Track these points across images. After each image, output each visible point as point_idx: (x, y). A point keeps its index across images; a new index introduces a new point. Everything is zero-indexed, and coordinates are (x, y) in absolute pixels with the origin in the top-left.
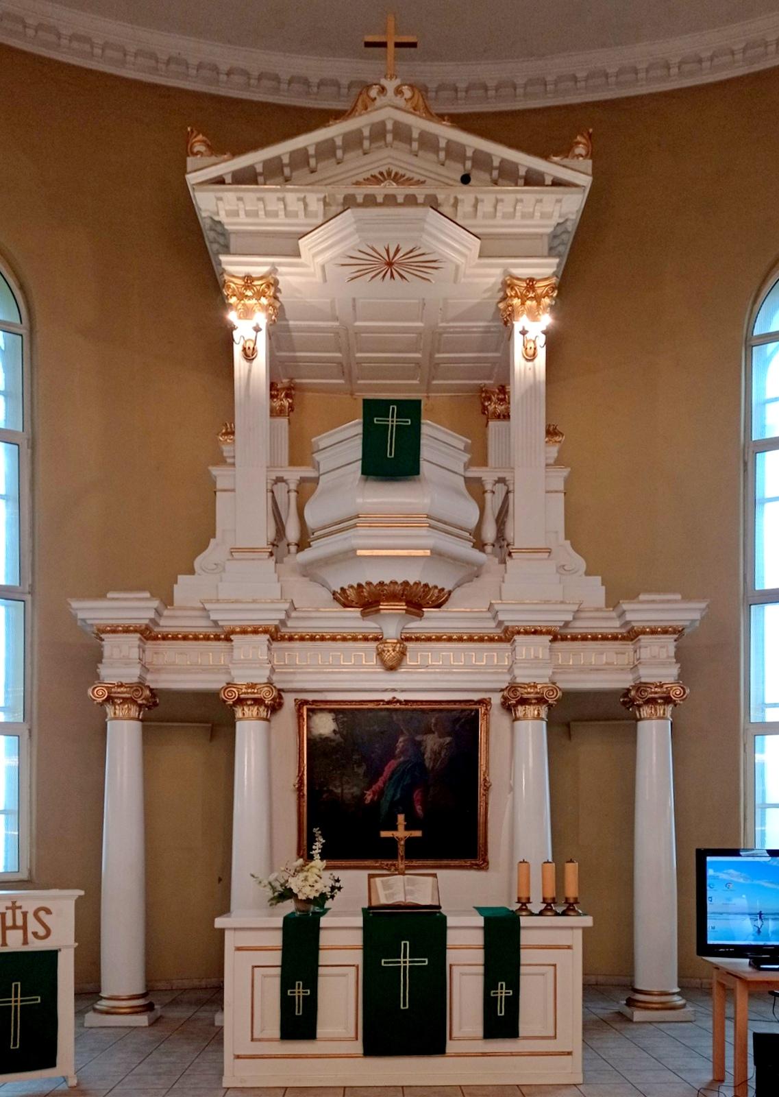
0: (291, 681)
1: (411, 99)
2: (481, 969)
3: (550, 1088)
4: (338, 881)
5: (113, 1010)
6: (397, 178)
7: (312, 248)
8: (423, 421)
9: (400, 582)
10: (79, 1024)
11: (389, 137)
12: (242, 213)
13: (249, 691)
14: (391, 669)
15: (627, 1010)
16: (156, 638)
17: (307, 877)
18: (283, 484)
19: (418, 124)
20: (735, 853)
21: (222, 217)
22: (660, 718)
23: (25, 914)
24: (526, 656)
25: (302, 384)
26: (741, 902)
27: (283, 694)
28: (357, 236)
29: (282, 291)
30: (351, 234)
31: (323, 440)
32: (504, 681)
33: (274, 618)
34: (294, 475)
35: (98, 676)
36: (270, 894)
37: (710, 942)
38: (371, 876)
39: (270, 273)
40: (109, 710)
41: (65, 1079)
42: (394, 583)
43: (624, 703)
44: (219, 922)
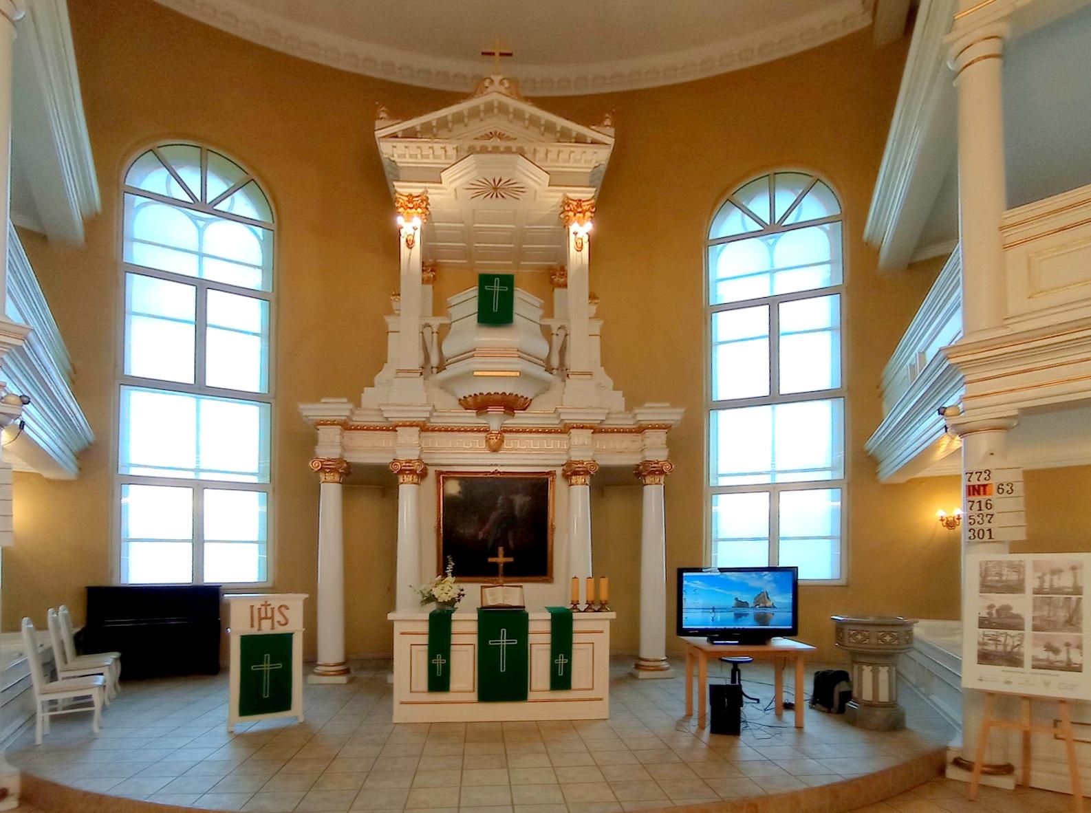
0: (433, 458)
1: (509, 88)
2: (549, 647)
3: (589, 722)
4: (462, 590)
5: (327, 673)
6: (500, 136)
7: (450, 178)
8: (515, 288)
10: (305, 682)
11: (496, 111)
12: (407, 156)
13: (407, 464)
15: (635, 671)
16: (350, 429)
17: (443, 587)
18: (430, 328)
19: (514, 104)
20: (700, 570)
21: (396, 158)
22: (657, 484)
23: (273, 609)
25: (440, 262)
26: (701, 602)
27: (427, 467)
28: (475, 171)
29: (431, 204)
30: (473, 170)
31: (454, 300)
32: (563, 459)
33: (423, 416)
34: (436, 322)
35: (314, 453)
36: (420, 598)
37: (684, 627)
38: (474, 645)
39: (423, 193)
40: (322, 476)
41: (297, 718)
42: (496, 393)
43: (636, 474)
44: (391, 616)
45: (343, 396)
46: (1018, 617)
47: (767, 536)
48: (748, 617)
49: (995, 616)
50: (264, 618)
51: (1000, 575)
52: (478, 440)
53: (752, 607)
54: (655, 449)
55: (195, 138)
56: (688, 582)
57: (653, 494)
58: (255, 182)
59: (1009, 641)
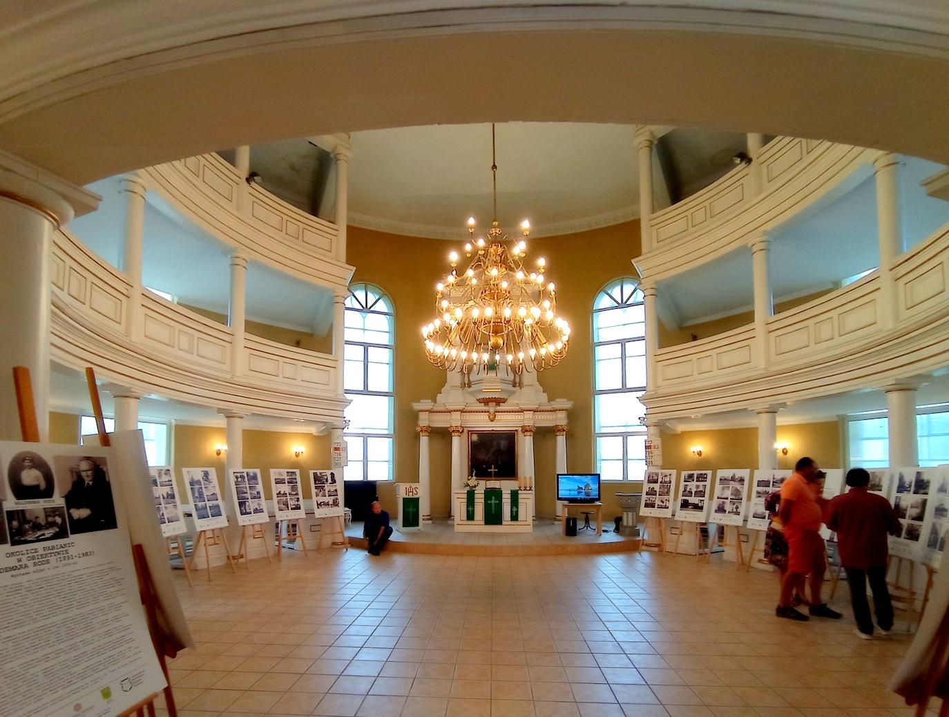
14: (492, 421)
45: (429, 399)
52: (485, 417)
54: (561, 419)
55: (364, 280)
57: (561, 440)
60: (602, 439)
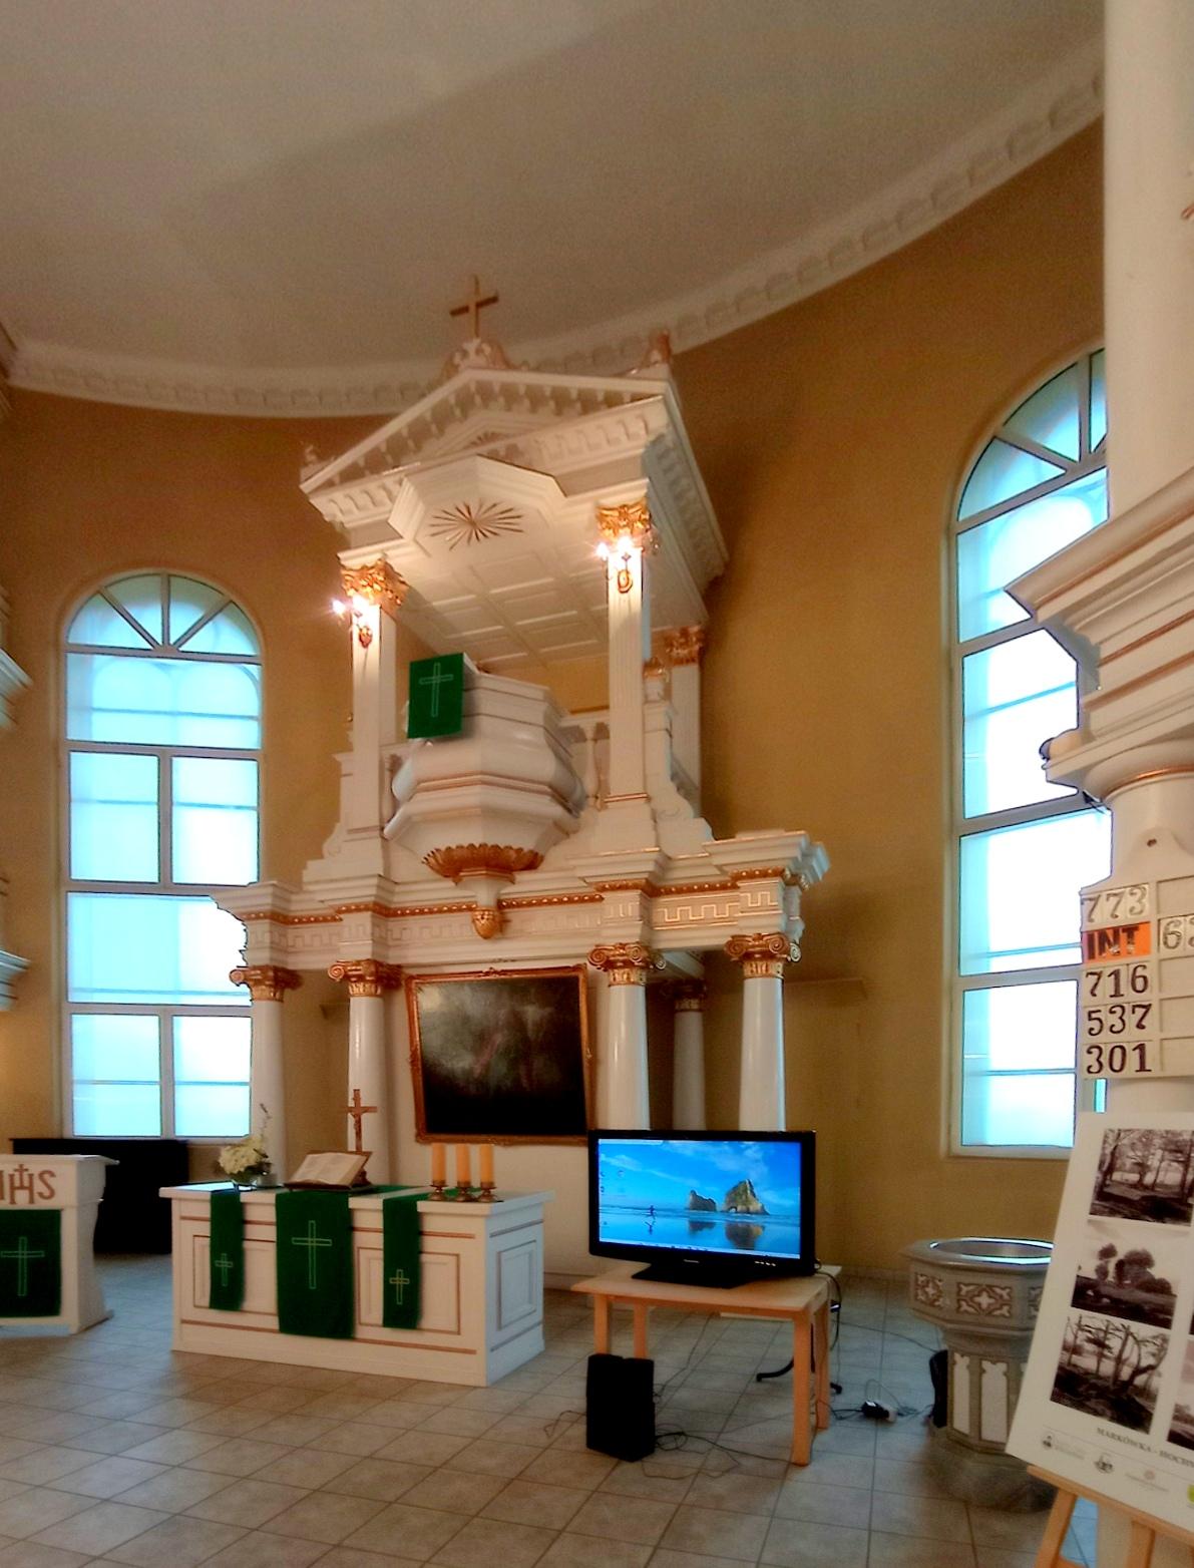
2: (380, 1254)
9: (466, 845)
23: (31, 1176)
24: (725, 908)
37: (601, 1240)
42: (460, 847)
46: (1163, 1288)
47: (1072, 1065)
48: (714, 1230)
49: (1111, 1278)
50: (18, 1188)
51: (1142, 1167)
53: (722, 1212)
55: (152, 563)
56: (607, 1156)
58: (235, 603)
59: (1131, 1354)
60: (995, 996)
